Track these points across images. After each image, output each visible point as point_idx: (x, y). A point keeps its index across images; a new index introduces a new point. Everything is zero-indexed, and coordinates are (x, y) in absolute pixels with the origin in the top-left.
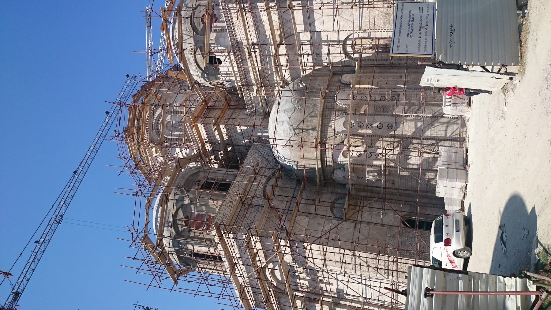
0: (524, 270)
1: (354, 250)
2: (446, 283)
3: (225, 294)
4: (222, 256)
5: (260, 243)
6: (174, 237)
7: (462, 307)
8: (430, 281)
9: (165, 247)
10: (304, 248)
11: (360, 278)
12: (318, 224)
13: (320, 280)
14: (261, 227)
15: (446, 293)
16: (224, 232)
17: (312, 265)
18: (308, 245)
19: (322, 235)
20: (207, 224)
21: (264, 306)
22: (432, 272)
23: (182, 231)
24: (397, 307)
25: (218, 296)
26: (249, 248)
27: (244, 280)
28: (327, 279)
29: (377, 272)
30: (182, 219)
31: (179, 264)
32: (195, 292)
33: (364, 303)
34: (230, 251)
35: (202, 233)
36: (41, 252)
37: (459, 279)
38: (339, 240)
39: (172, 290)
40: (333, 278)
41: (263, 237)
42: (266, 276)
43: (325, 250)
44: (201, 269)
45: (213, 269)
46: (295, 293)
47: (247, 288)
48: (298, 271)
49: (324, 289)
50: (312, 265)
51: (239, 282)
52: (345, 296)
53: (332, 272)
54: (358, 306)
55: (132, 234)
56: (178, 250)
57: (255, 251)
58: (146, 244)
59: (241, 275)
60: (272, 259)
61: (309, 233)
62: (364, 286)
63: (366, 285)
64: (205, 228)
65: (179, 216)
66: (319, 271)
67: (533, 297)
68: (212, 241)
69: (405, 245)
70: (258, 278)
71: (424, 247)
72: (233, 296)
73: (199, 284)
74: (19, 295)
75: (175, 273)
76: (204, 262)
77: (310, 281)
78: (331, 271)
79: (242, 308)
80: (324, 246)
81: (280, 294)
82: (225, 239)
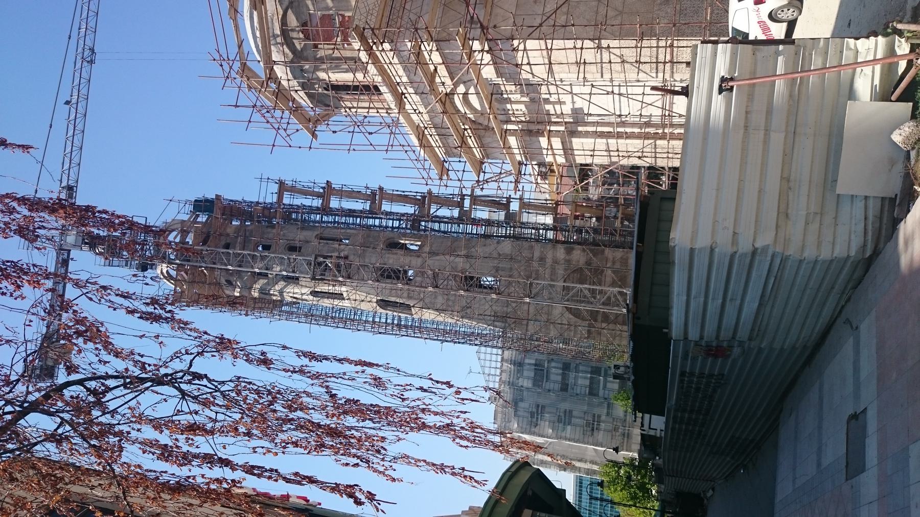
0: (893, 22)
1: (599, 39)
2: (756, 64)
3: (396, 143)
4: (378, 84)
5: (438, 53)
6: (292, 62)
7: (780, 101)
8: (728, 64)
9: (282, 81)
10: (514, 50)
11: (611, 84)
13: (544, 99)
14: (435, 24)
15: (755, 81)
16: (373, 42)
17: (530, 76)
18: (519, 44)
19: (543, 20)
20: (343, 32)
21: (459, 154)
22: (732, 49)
23: (302, 49)
24: (672, 122)
25: (385, 148)
26: (420, 63)
27: (422, 119)
28: (556, 96)
29: (639, 69)
30: (297, 29)
31: (311, 106)
32: (348, 147)
33: (617, 123)
34: (391, 75)
35: (337, 49)
36: (81, 119)
37: (778, 54)
38: (573, 25)
39: (310, 148)
40: (565, 92)
41: (441, 42)
42: (455, 107)
43: (549, 48)
44: (350, 110)
45: (369, 108)
46: (505, 127)
47: (429, 131)
48: (506, 91)
49: (552, 112)
50: (530, 76)
51: (414, 123)
52: (586, 118)
53: (564, 83)
54: (608, 131)
55: (221, 65)
56: (303, 83)
57: (432, 68)
58: (248, 80)
59: (415, 110)
60: (462, 78)
61: (519, 22)
62: (618, 96)
63: (620, 94)
64: (339, 39)
65: (290, 22)
66: (542, 85)
67: (903, 65)
68: (356, 60)
69: (686, 14)
70: (444, 112)
71: (718, 13)
72: (409, 146)
73: (351, 134)
74: (73, 190)
75: (310, 121)
76: (351, 97)
77: (528, 104)
78: (561, 81)
79: (425, 160)
80: (547, 41)
81: (482, 131)
82: (378, 53)
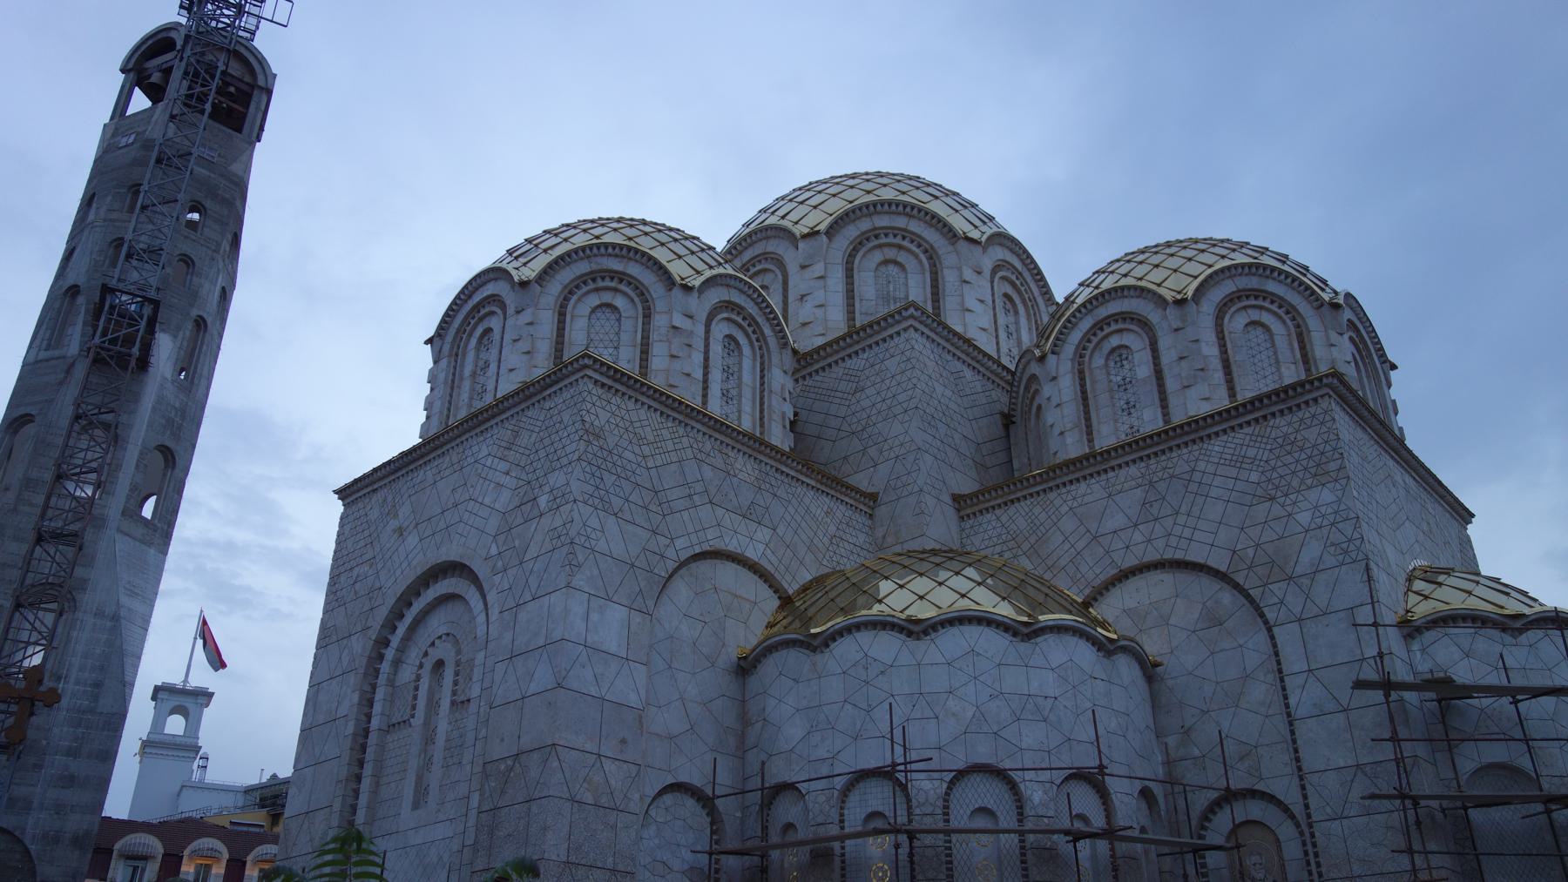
12: (623, 741)
